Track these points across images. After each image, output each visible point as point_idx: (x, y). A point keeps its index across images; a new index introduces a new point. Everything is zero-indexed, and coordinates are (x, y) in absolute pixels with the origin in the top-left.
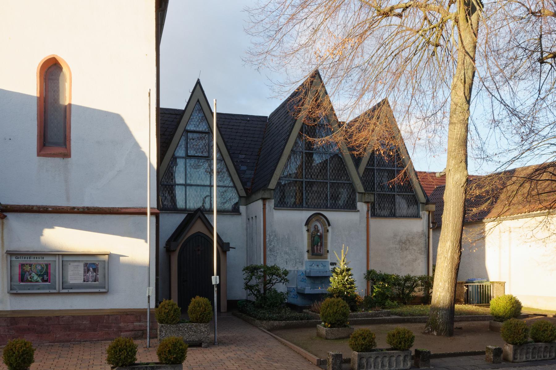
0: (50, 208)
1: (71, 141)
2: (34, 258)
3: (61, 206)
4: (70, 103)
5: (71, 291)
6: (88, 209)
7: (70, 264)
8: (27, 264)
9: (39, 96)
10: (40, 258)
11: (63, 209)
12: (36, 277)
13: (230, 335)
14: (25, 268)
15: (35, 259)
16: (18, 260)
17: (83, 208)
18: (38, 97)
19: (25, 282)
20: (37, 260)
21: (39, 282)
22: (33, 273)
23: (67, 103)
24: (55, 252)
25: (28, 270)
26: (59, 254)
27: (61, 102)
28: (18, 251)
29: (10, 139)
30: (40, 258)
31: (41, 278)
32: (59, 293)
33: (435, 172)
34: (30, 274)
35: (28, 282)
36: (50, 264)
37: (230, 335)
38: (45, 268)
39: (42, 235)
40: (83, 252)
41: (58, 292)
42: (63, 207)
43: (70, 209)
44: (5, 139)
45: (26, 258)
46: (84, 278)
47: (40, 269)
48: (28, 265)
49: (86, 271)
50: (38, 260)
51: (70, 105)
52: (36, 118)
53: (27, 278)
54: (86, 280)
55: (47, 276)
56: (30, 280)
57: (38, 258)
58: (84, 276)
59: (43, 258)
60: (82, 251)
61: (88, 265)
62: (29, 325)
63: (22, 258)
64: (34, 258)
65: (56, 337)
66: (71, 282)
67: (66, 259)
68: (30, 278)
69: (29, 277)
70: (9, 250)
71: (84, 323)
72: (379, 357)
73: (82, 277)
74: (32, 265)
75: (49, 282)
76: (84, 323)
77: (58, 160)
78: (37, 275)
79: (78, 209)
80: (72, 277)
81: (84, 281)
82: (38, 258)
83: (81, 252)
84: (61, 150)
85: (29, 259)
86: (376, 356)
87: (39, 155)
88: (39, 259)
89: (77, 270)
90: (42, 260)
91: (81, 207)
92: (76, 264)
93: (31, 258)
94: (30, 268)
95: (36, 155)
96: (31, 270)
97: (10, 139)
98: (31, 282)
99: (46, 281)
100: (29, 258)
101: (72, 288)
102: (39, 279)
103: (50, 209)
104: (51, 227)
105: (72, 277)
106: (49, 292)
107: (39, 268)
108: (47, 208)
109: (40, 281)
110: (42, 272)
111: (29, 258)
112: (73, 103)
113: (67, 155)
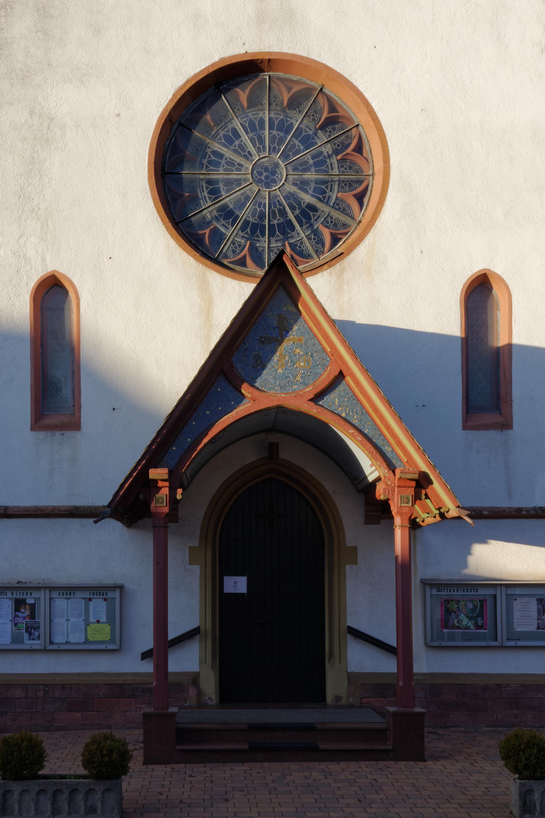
0: (485, 511)
1: (513, 403)
2: (464, 590)
3: (500, 508)
4: (510, 342)
5: (520, 644)
6: (542, 510)
7: (515, 600)
8: (452, 601)
9: (463, 336)
10: (472, 590)
11: (504, 511)
12: (465, 621)
13: (221, 747)
14: (449, 606)
15: (466, 593)
16: (440, 593)
17: (534, 509)
18: (462, 338)
19: (450, 629)
20: (467, 593)
21: (471, 629)
22: (462, 615)
23: (502, 342)
24: (470, 580)
25: (455, 610)
26: (501, 585)
27: (490, 344)
28: (438, 580)
29: (424, 406)
30: (472, 590)
31: (474, 622)
32: (502, 647)
33: (49, 598)
34: (458, 616)
35: (454, 629)
36: (486, 600)
37: (221, 747)
38: (479, 607)
39: (469, 553)
40: (533, 581)
41: (500, 645)
42: (504, 509)
43: (515, 511)
44: (417, 406)
45: (452, 591)
46: (538, 623)
47: (471, 608)
48: (454, 602)
49: (542, 611)
50: (469, 593)
51: (510, 346)
52: (460, 370)
53: (453, 622)
54: (540, 627)
55: (482, 619)
56: (457, 625)
57: (469, 591)
58: (538, 620)
59: (477, 590)
60: (531, 579)
61: (543, 602)
62: (456, 697)
63: (446, 590)
64: (464, 590)
65: (497, 718)
66: (517, 630)
67: (511, 591)
68: (458, 622)
69: (456, 621)
70: (424, 578)
71: (539, 696)
72: (94, 790)
73: (536, 622)
74: (459, 601)
75: (486, 629)
76: (539, 696)
77: (493, 434)
78: (468, 617)
79: (528, 511)
80: (519, 620)
81: (538, 628)
82: (469, 591)
83: (531, 581)
84: (495, 418)
85: (456, 593)
86: (87, 789)
87: (465, 427)
88: (454, 592)
89: (527, 609)
90: (476, 593)
91: (530, 508)
92: (526, 599)
93: (459, 590)
94: (457, 606)
95: (461, 428)
96: (459, 610)
97: (424, 406)
98: (459, 628)
99: (481, 627)
100: (456, 590)
101: (519, 640)
102: (470, 624)
103: (485, 513)
104: (483, 541)
105: (519, 620)
106: (487, 645)
107: (470, 606)
108: (481, 512)
109: (472, 627)
110: (475, 613)
111: (456, 590)
112: (515, 341)
113: (507, 425)
